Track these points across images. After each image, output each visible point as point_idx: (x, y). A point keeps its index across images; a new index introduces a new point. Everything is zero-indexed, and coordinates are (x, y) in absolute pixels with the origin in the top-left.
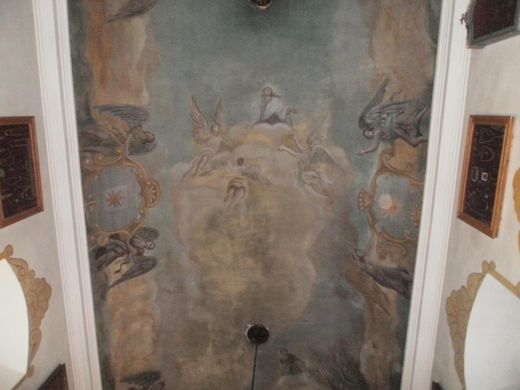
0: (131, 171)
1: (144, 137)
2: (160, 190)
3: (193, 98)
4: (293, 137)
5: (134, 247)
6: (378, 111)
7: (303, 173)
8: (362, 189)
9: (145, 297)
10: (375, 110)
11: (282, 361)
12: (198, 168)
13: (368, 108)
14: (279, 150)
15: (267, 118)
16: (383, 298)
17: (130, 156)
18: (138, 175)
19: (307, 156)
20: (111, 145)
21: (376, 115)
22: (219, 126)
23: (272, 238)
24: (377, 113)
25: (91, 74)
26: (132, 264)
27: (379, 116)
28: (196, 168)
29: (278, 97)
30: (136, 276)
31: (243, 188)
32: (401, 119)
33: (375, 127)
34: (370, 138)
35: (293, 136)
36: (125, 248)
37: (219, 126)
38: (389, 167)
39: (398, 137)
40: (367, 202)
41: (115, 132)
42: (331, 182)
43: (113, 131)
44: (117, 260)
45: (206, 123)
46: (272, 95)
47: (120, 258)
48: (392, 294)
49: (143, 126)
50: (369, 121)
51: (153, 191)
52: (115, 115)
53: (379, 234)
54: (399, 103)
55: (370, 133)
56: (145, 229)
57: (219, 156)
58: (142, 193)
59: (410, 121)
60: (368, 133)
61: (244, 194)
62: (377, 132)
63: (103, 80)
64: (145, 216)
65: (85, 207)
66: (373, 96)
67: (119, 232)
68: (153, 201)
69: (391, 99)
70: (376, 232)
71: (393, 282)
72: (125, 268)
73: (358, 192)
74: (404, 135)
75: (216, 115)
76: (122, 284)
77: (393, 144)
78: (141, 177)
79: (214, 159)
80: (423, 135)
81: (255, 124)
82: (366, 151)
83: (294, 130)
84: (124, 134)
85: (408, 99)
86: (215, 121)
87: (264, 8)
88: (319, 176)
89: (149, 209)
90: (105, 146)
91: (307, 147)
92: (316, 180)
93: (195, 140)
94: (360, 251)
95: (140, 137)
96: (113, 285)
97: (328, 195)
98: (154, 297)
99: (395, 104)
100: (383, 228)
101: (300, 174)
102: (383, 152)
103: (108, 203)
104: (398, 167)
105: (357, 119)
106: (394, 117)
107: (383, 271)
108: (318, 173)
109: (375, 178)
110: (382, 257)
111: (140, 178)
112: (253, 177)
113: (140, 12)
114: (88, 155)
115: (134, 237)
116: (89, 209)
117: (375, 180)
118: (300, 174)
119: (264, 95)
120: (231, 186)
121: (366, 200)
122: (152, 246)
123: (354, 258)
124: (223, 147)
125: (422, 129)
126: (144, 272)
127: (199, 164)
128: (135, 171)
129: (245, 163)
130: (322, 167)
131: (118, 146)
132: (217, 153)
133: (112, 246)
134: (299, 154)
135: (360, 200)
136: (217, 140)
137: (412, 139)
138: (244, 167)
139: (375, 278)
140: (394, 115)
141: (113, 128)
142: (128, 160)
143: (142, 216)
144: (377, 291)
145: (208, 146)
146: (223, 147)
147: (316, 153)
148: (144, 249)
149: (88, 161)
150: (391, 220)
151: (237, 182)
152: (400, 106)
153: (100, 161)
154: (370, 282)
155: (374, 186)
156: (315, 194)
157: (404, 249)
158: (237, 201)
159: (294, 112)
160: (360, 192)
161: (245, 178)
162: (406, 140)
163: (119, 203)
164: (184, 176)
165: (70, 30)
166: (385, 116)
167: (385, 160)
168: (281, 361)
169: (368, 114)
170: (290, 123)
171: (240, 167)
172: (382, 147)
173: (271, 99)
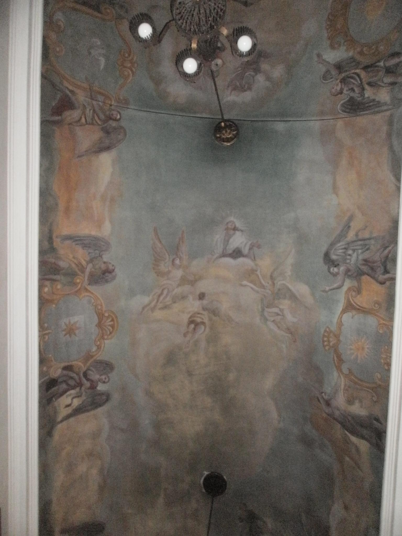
0: (89, 302)
1: (103, 267)
2: (117, 322)
3: (155, 230)
4: (255, 272)
5: (88, 380)
6: (343, 247)
7: (266, 309)
8: (328, 327)
9: (95, 435)
10: (341, 246)
11: (241, 520)
12: (158, 301)
13: (332, 244)
14: (242, 285)
15: (230, 252)
16: (353, 450)
17: (89, 286)
18: (96, 306)
19: (270, 292)
20: (71, 274)
21: (341, 251)
22: (181, 258)
23: (232, 376)
24: (342, 249)
25: (57, 204)
26: (84, 398)
27: (344, 253)
28: (155, 301)
29: (242, 231)
30: (88, 411)
31: (203, 323)
32: (367, 255)
33: (340, 264)
34: (335, 275)
35: (257, 271)
36: (78, 381)
37: (181, 258)
38: (355, 305)
39: (364, 273)
40: (333, 341)
41: (75, 261)
42: (295, 320)
43: (73, 260)
44: (68, 393)
45: (167, 256)
46: (235, 229)
47: (72, 392)
48: (363, 446)
49: (104, 256)
50: (334, 257)
51: (110, 323)
52: (77, 244)
53: (346, 376)
54: (364, 240)
55: (336, 270)
56: (101, 362)
57: (178, 291)
58: (99, 325)
59: (377, 257)
60: (333, 270)
61: (205, 330)
62: (342, 268)
63: (67, 210)
64: (101, 347)
65: (39, 336)
66: (338, 232)
67: (74, 363)
68: (111, 333)
69: (357, 235)
70: (343, 373)
71: (365, 432)
72: (76, 403)
73: (322, 331)
74: (370, 271)
75: (178, 248)
76: (72, 420)
77: (359, 281)
78: (100, 307)
79: (174, 292)
80: (391, 272)
81: (217, 258)
82: (332, 287)
83: (256, 265)
84: (84, 263)
85: (374, 235)
86: (177, 255)
87: (229, 144)
88: (282, 313)
89: (105, 341)
90: (65, 275)
91: (270, 282)
92: (279, 317)
93: (156, 272)
94: (325, 394)
95: (100, 268)
96: (62, 421)
97: (291, 333)
98: (105, 435)
99: (360, 240)
100: (350, 370)
101: (263, 310)
102: (349, 289)
103: (64, 333)
104: (365, 305)
105: (322, 255)
106: (359, 253)
107: (353, 418)
108: (282, 310)
109: (341, 316)
110: (350, 402)
111: (98, 309)
112: (214, 312)
113: (108, 148)
114: (48, 283)
115: (88, 369)
116: (44, 338)
117: (341, 319)
118: (263, 310)
119: (227, 229)
120: (191, 322)
121: (331, 339)
122: (107, 380)
123: (319, 401)
124: (184, 281)
125: (389, 266)
126: (96, 407)
127: (159, 296)
128: (93, 301)
129: (206, 298)
130: (285, 304)
131: (79, 275)
132: (177, 287)
133: (64, 378)
134: (263, 290)
135: (325, 339)
136: (179, 273)
137: (379, 276)
138: (205, 302)
139: (344, 426)
140: (360, 251)
141: (74, 258)
142: (87, 290)
143: (98, 348)
144: (347, 441)
145: (168, 279)
146: (184, 281)
147: (279, 290)
148: (98, 382)
149: (46, 290)
150: (359, 361)
151: (198, 317)
152: (367, 242)
153: (58, 289)
154: (338, 432)
155: (340, 324)
156: (278, 331)
157: (374, 394)
158: (197, 336)
159: (257, 247)
160: (325, 331)
161: (205, 313)
162: (373, 278)
163: (75, 334)
164: (143, 308)
165: (41, 165)
166: (350, 252)
167: (351, 298)
168: (240, 518)
169: (333, 250)
170: (253, 258)
171: (201, 301)
172: (348, 284)
173: (234, 234)
